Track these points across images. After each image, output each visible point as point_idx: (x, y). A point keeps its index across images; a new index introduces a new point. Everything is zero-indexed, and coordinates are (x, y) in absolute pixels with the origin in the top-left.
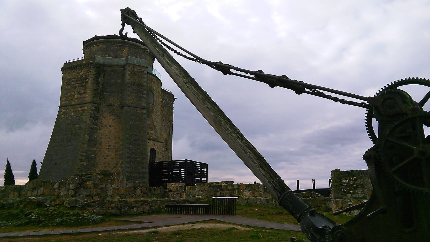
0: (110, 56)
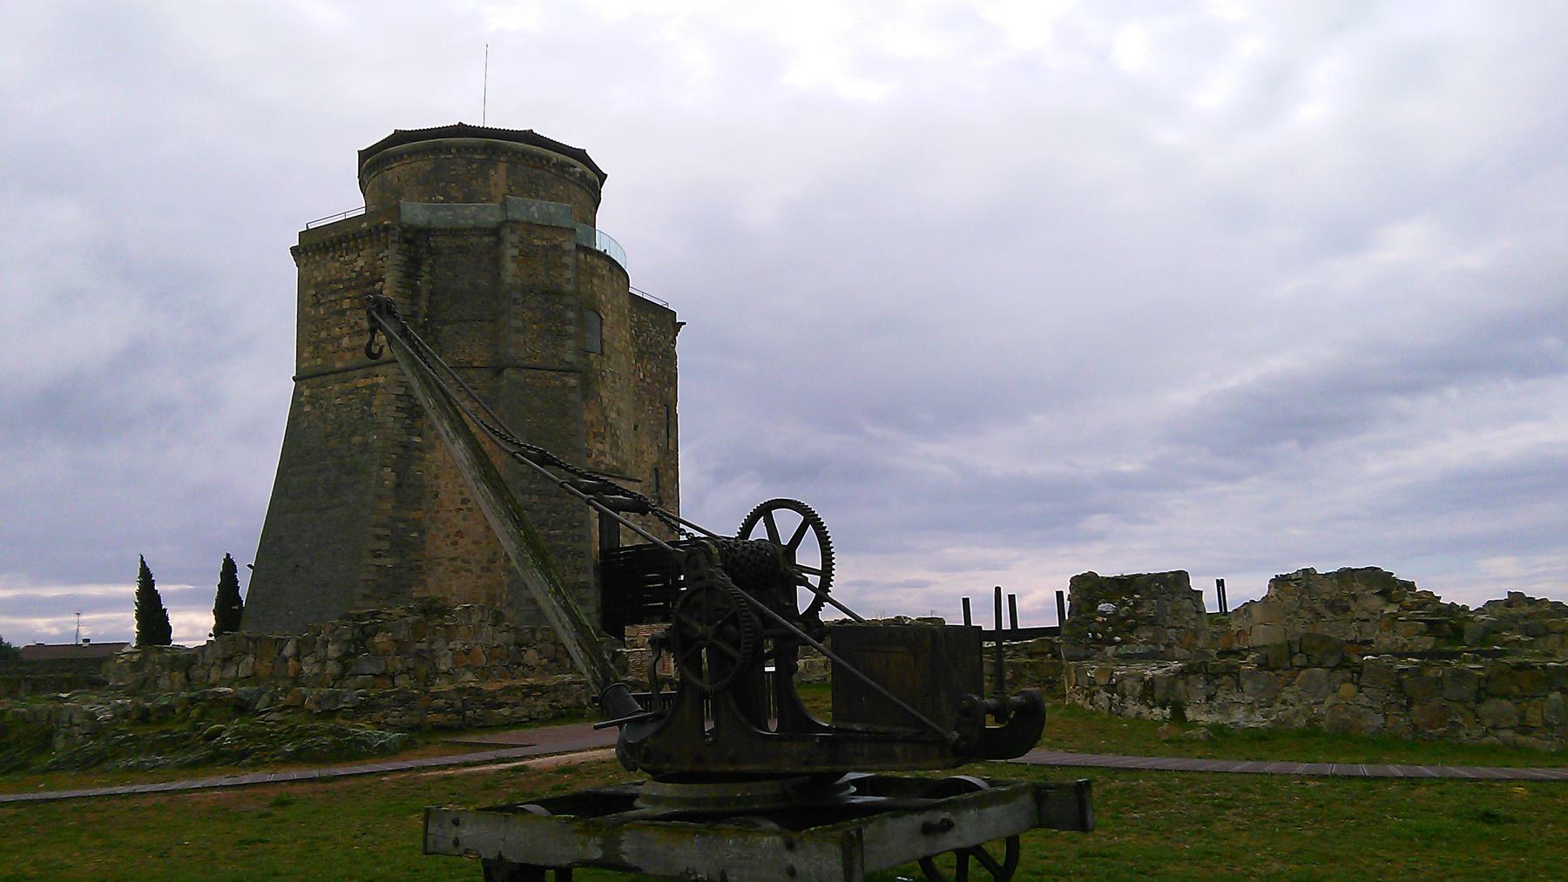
0: (449, 198)
